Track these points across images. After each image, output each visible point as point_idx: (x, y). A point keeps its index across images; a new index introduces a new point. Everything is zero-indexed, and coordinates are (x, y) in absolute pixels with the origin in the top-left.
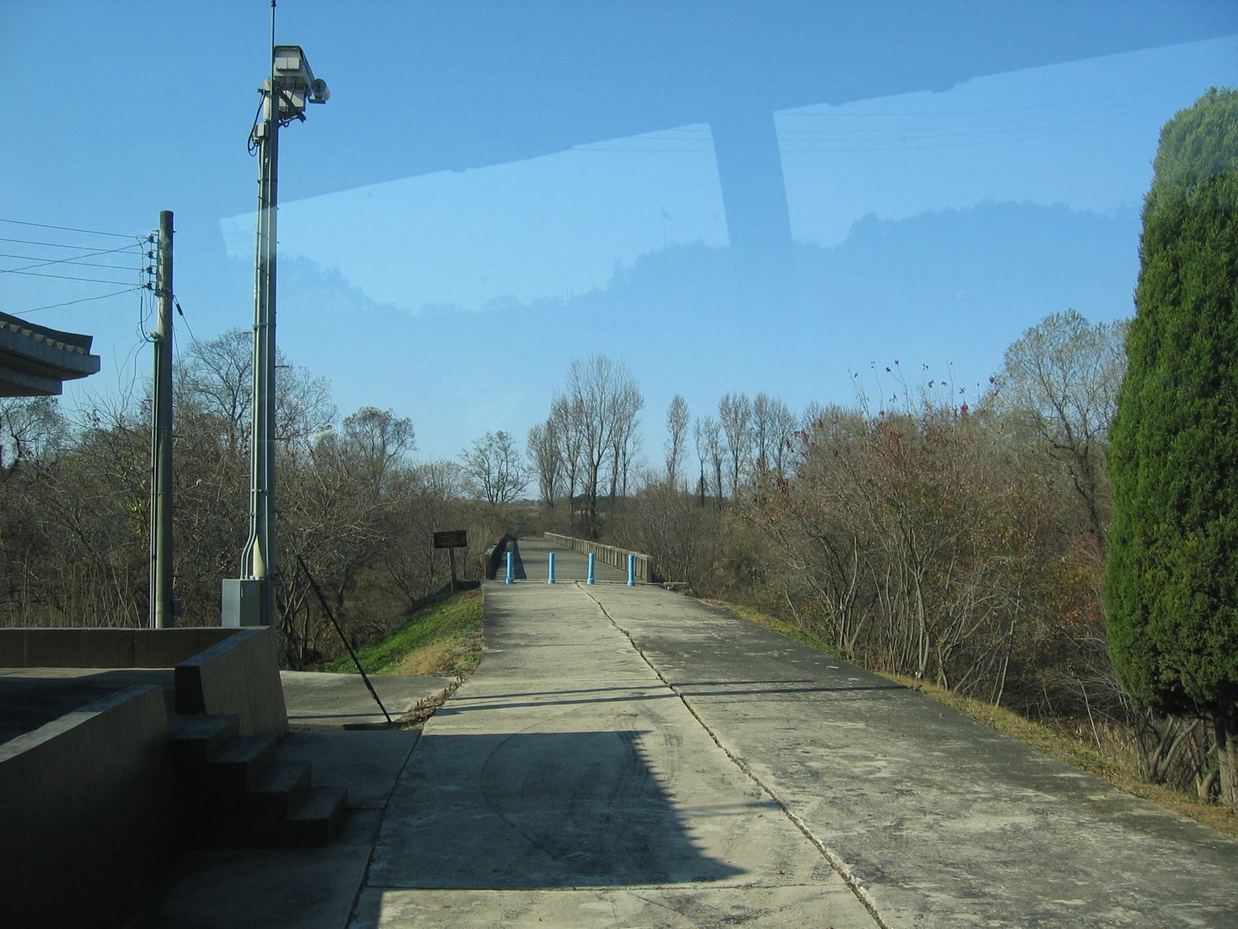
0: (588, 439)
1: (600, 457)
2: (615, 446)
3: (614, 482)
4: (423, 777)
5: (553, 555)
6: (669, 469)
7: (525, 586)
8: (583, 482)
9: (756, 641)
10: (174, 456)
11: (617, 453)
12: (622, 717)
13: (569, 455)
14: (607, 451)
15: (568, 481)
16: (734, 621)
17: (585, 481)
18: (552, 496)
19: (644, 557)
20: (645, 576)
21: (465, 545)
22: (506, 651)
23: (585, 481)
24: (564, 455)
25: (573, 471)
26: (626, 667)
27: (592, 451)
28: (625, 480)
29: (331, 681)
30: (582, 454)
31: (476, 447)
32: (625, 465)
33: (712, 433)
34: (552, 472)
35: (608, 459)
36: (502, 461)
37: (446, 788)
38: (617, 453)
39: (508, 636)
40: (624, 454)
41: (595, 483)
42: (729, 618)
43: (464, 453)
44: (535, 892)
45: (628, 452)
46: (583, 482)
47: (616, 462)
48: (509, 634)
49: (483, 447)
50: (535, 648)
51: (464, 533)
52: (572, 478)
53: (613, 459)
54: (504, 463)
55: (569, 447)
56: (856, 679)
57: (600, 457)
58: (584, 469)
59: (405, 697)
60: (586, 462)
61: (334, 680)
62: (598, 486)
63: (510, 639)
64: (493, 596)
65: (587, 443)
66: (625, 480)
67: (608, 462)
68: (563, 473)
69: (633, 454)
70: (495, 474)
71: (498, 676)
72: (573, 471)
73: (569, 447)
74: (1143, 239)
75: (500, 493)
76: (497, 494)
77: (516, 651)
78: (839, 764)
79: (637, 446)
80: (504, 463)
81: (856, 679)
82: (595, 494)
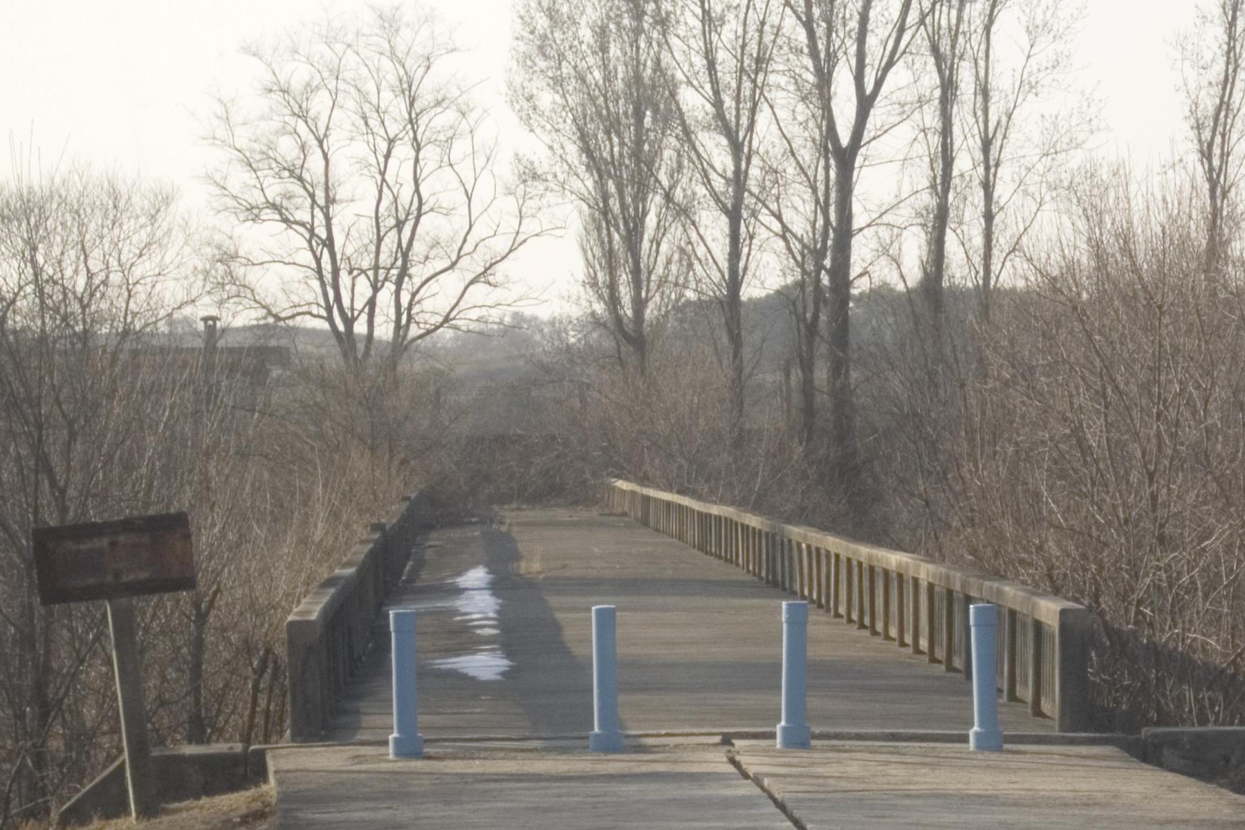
0: (809, 25)
1: (865, 104)
2: (935, 49)
3: (940, 221)
5: (607, 619)
6: (1206, 154)
8: (785, 233)
10: (1212, 124)
11: (948, 87)
13: (718, 103)
14: (898, 77)
15: (714, 226)
17: (799, 226)
18: (639, 304)
19: (1049, 610)
20: (1051, 706)
21: (187, 583)
23: (799, 226)
24: (693, 102)
25: (739, 180)
27: (824, 79)
28: (989, 217)
30: (778, 97)
32: (986, 144)
34: (642, 183)
35: (905, 117)
38: (948, 87)
40: (984, 92)
41: (844, 234)
45: (1002, 80)
46: (785, 233)
47: (946, 131)
49: (298, 75)
51: (44, 538)
52: (734, 216)
53: (931, 117)
54: (403, 151)
55: (711, 66)
57: (865, 104)
58: (791, 170)
60: (794, 130)
62: (862, 250)
65: (801, 36)
66: (989, 217)
67: (906, 132)
68: (690, 187)
69: (1027, 86)
72: (739, 180)
73: (711, 66)
75: (385, 297)
76: (372, 303)
79: (1045, 50)
80: (403, 151)
82: (848, 284)
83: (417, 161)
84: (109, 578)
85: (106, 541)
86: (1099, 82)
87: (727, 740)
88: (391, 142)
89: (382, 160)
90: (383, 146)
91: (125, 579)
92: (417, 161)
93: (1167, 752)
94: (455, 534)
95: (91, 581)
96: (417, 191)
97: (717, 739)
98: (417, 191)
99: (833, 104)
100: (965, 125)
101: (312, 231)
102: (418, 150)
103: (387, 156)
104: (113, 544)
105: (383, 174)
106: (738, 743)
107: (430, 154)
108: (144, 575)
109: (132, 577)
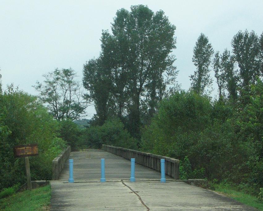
54: (68, 92)
80: (68, 92)
83: (70, 93)
84: (25, 154)
85: (24, 148)
86: (32, 86)
87: (122, 180)
88: (66, 90)
89: (65, 93)
90: (65, 91)
91: (27, 154)
92: (70, 93)
93: (192, 183)
94: (76, 152)
95: (22, 154)
96: (70, 98)
97: (121, 180)
98: (70, 98)
99: (216, 78)
100: (128, 203)
101: (53, 104)
102: (70, 92)
103: (66, 93)
104: (25, 148)
105: (65, 95)
106: (124, 181)
107: (72, 92)
108: (30, 153)
109: (28, 153)
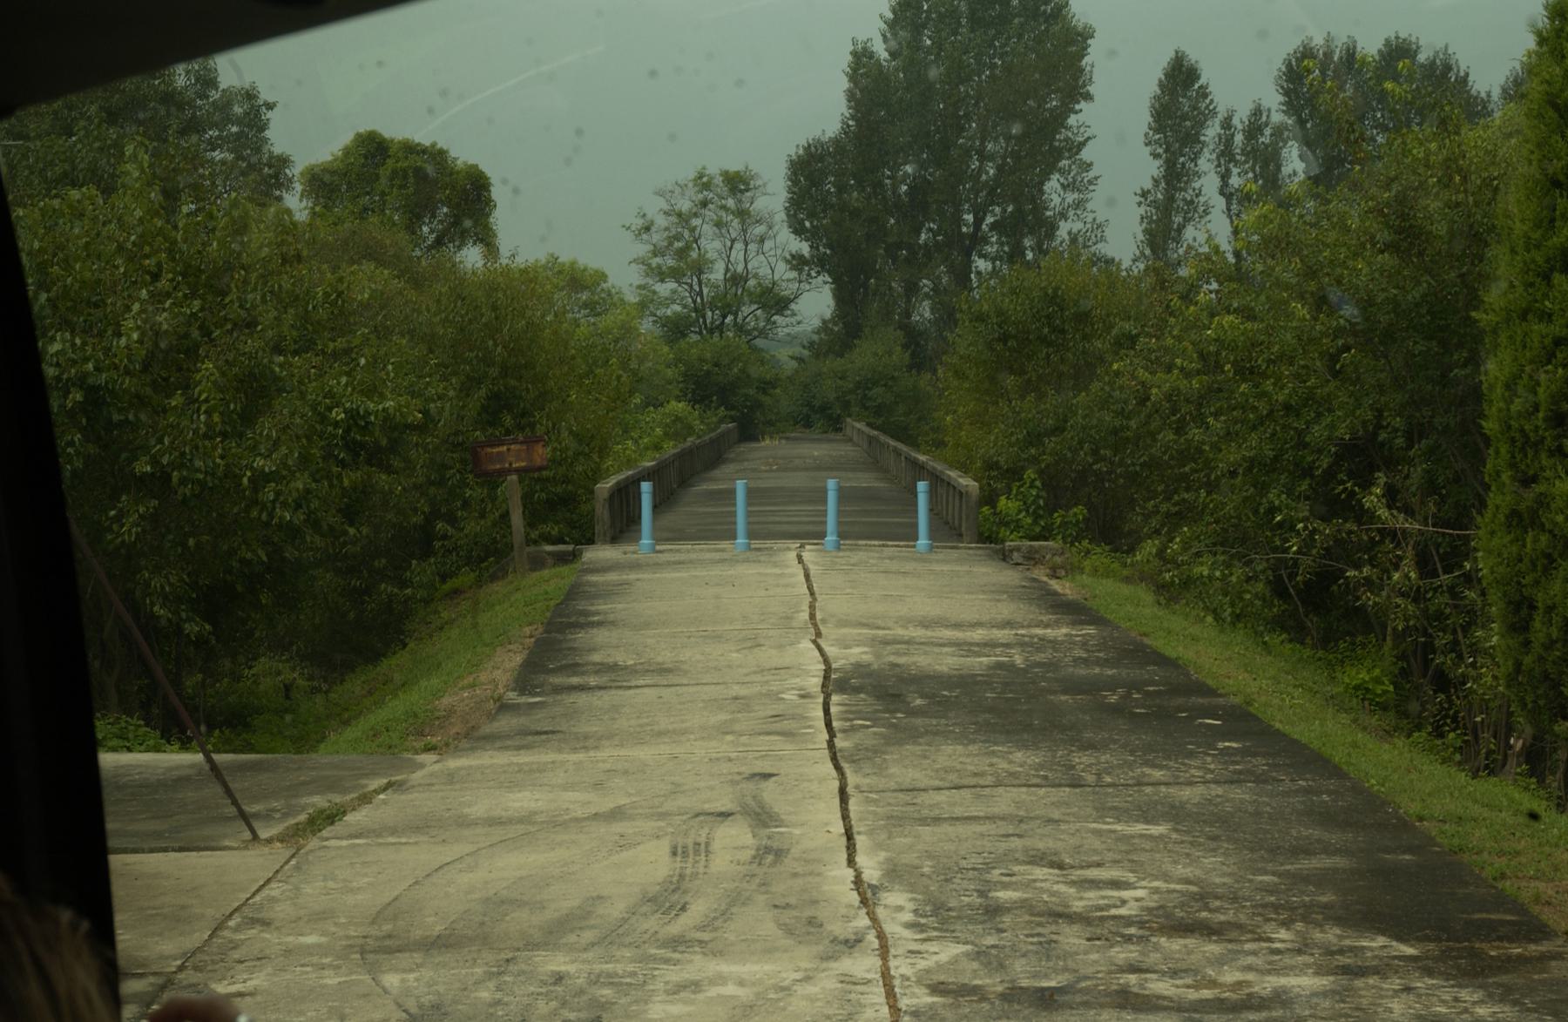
4: (266, 924)
7: (677, 557)
9: (1097, 670)
12: (702, 818)
16: (1090, 630)
22: (550, 699)
26: (778, 726)
29: (170, 769)
31: (666, 207)
33: (1267, 162)
36: (733, 241)
37: (302, 939)
39: (574, 668)
42: (1082, 623)
43: (640, 222)
44: (104, 783)
48: (577, 665)
49: (685, 205)
50: (613, 692)
54: (739, 246)
56: (1234, 745)
59: (311, 794)
61: (178, 768)
63: (575, 674)
64: (594, 585)
70: (717, 274)
71: (507, 748)
74: (1398, 52)
77: (569, 699)
78: (1053, 894)
80: (739, 246)
81: (1234, 745)
